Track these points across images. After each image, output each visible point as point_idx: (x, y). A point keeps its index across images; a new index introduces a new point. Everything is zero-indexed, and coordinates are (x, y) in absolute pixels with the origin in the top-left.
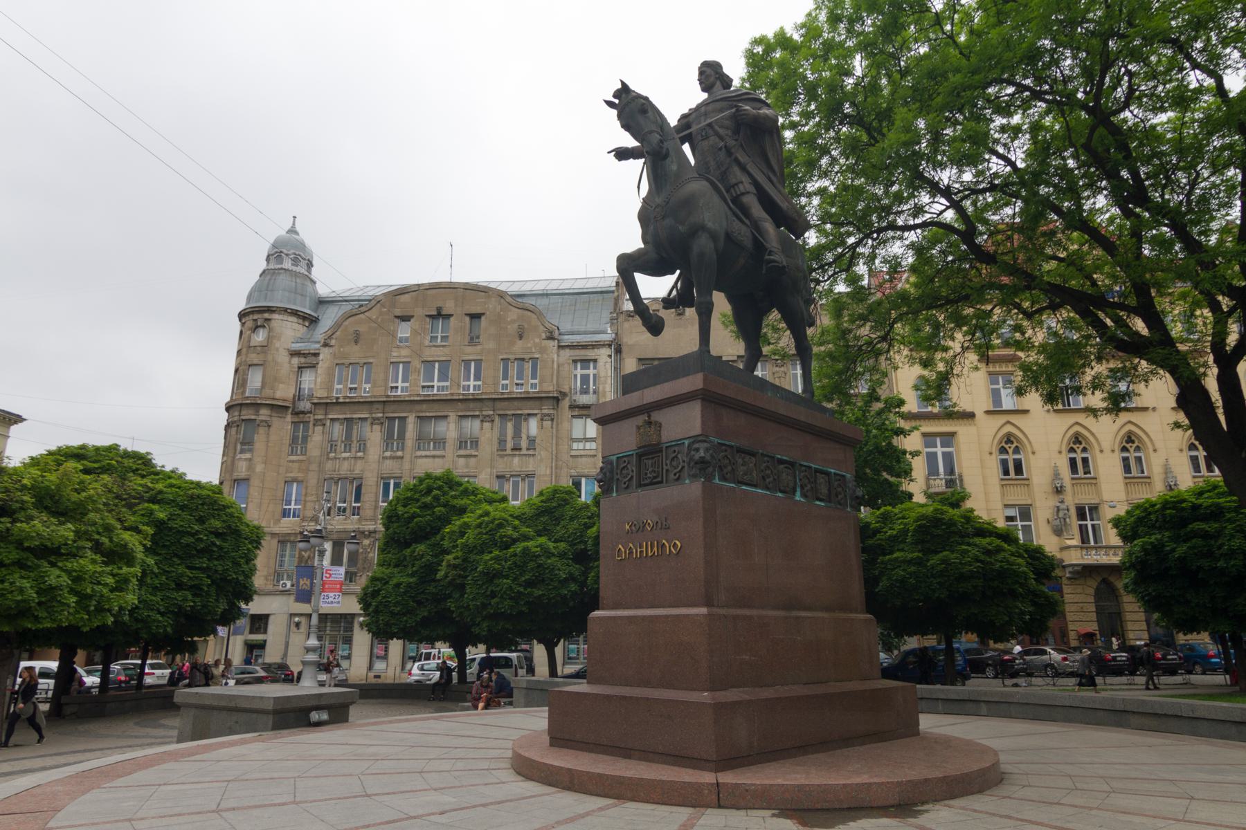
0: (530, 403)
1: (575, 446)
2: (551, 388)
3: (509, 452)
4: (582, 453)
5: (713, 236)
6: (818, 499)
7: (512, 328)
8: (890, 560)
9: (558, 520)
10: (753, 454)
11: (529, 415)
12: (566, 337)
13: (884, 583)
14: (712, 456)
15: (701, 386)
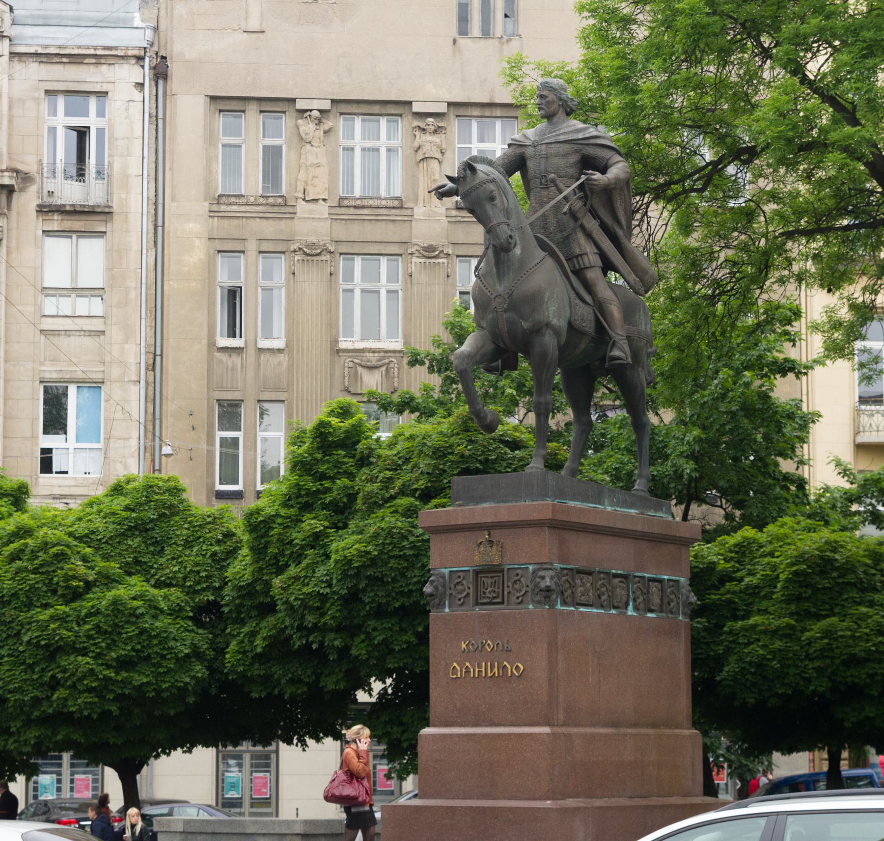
1: (50, 306)
4: (67, 324)
5: (556, 332)
6: (651, 611)
8: (743, 629)
9: (159, 546)
10: (590, 573)
12: (29, 31)
13: (731, 667)
14: (556, 584)
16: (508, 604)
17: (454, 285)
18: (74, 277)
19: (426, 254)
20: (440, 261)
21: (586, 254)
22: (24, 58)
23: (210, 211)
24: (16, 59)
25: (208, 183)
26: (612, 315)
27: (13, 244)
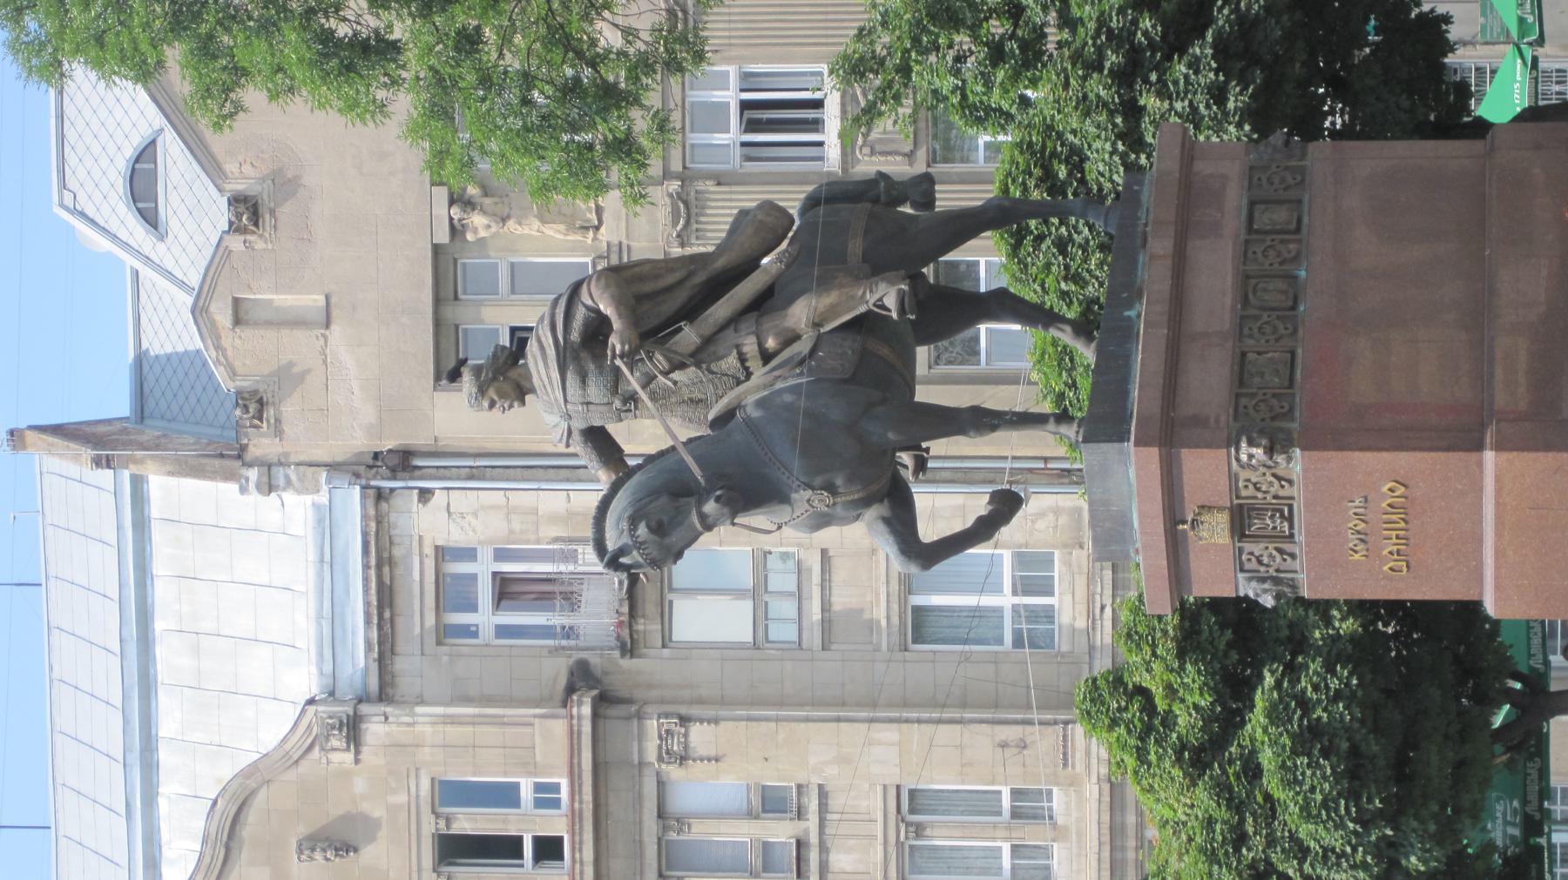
0: (617, 807)
2: (559, 727)
11: (661, 814)
18: (738, 593)
22: (388, 678)
24: (390, 691)
27: (687, 694)
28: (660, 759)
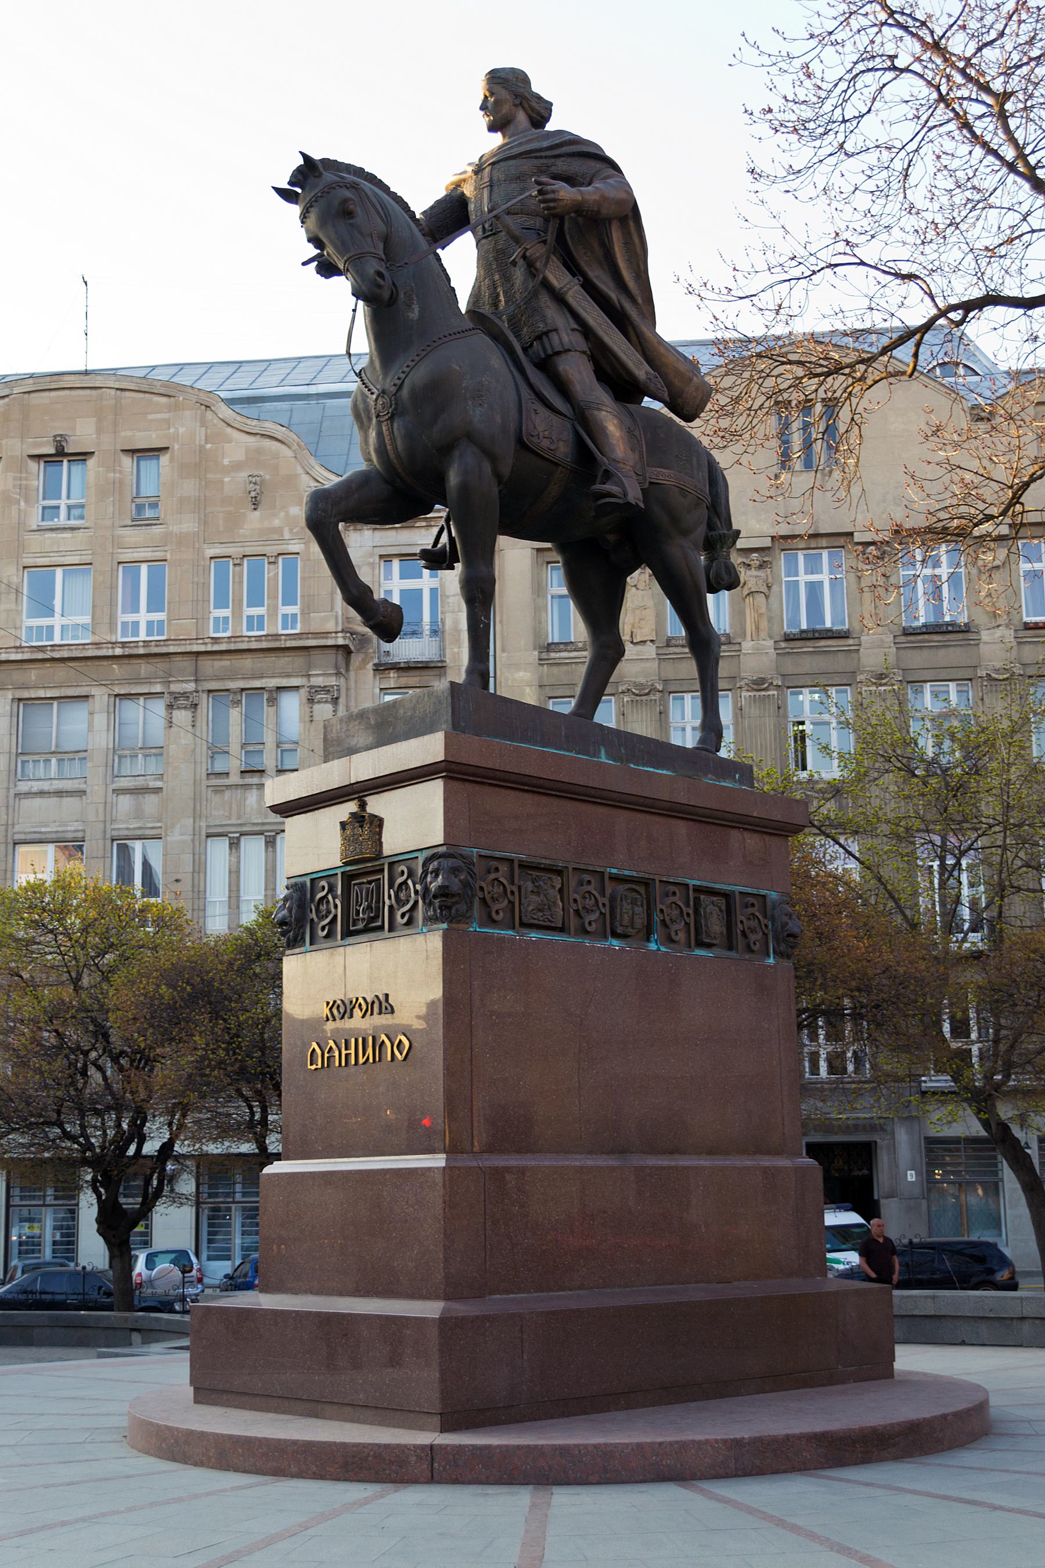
0: (283, 662)
2: (330, 626)
3: (235, 779)
7: (235, 483)
11: (279, 689)
15: (441, 757)
16: (390, 930)
17: (786, 716)
19: (755, 687)
20: (770, 693)
21: (556, 330)
23: (540, 660)
25: (538, 631)
26: (604, 429)
28: (312, 687)
